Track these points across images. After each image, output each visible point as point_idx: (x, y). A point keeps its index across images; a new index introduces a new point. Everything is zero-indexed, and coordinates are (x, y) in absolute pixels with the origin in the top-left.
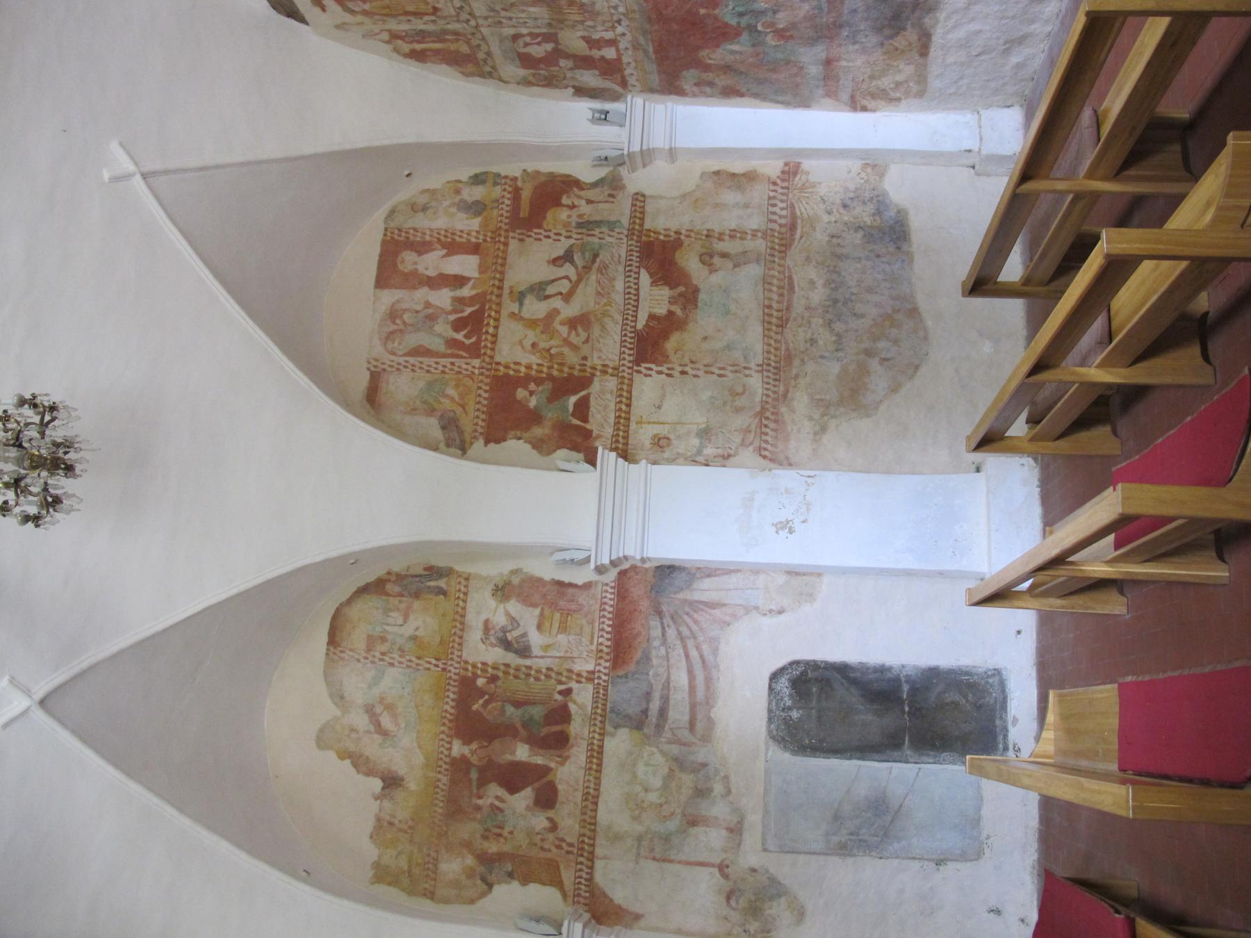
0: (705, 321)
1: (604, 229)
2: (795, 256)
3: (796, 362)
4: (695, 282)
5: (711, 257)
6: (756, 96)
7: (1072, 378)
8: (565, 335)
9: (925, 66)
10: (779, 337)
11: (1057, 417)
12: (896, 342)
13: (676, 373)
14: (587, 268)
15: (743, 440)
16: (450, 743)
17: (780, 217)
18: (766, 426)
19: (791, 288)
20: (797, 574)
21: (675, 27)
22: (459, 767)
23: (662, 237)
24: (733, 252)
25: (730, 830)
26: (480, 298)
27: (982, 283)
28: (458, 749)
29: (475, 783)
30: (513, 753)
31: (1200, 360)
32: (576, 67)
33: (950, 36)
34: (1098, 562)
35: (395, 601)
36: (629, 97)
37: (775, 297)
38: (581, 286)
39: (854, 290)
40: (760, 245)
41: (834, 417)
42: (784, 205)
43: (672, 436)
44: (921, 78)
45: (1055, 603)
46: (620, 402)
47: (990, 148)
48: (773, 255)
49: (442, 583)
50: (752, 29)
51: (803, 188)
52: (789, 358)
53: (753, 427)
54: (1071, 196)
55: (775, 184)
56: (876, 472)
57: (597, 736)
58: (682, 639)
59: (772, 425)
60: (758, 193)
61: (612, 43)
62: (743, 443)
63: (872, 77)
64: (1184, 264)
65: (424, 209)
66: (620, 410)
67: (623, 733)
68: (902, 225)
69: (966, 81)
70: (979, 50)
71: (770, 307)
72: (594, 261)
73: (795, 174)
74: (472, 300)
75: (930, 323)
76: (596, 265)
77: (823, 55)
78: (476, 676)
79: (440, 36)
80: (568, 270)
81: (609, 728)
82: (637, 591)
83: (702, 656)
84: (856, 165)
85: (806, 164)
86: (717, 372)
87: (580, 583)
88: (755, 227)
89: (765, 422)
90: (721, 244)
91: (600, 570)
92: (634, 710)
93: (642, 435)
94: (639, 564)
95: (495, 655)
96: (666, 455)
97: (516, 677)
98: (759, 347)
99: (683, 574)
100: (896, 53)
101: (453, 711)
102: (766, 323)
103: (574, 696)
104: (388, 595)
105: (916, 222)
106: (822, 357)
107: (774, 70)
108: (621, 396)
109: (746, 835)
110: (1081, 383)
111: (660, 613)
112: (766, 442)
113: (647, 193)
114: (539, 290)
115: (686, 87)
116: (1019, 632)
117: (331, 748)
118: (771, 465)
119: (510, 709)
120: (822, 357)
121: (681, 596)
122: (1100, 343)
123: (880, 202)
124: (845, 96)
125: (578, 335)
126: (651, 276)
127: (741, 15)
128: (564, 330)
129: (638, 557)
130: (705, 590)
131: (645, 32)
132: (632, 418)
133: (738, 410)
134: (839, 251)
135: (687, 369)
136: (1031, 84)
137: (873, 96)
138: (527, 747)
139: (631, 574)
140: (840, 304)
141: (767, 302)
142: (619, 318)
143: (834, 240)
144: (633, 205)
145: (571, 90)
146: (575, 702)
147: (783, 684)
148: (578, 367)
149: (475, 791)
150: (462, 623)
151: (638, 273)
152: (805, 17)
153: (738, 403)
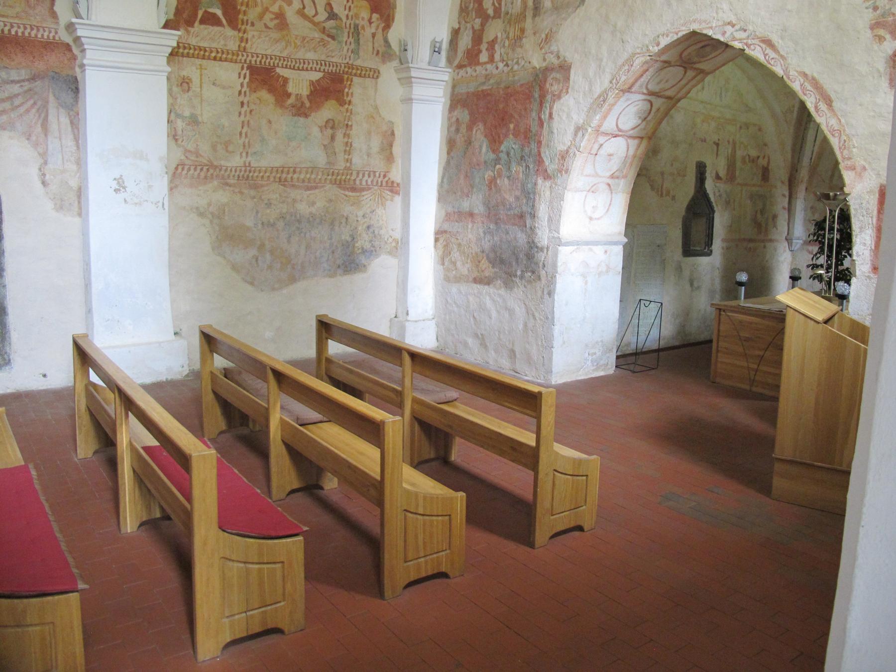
0: (284, 122)
1: (353, 46)
2: (333, 191)
3: (253, 193)
4: (313, 114)
5: (332, 128)
6: (448, 163)
7: (271, 400)
8: (271, 9)
9: (467, 282)
10: (272, 179)
11: (229, 389)
12: (270, 267)
13: (242, 98)
14: (323, 31)
15: (190, 151)
17: (361, 180)
18: (202, 169)
19: (308, 189)
20: (79, 197)
21: (501, 106)
23: (346, 90)
24: (335, 144)
27: (326, 328)
31: (289, 489)
32: (474, 31)
33: (488, 298)
34: (131, 435)
36: (450, 70)
37: (302, 176)
38: (310, 25)
39: (308, 235)
40: (341, 165)
41: (211, 222)
42: (369, 183)
43: (190, 93)
44: (458, 279)
45: (81, 403)
46: (218, 52)
47: (410, 327)
48: (333, 175)
50: (497, 161)
51: (381, 196)
52: (256, 187)
53: (200, 159)
54: (399, 389)
55: (385, 176)
56: (170, 258)
59: (203, 174)
60: (377, 164)
61: (491, 59)
62: (186, 151)
63: (459, 245)
64: (378, 478)
66: (211, 52)
68: (355, 269)
69: (456, 309)
70: (478, 317)
71: (294, 172)
72: (329, 36)
73: (392, 191)
75: (285, 291)
76: (326, 38)
77: (476, 211)
80: (322, 16)
82: (53, 60)
84: (397, 235)
85: (398, 199)
86: (244, 131)
87: (56, 8)
88: (354, 161)
89: (205, 168)
90: (342, 136)
91: (70, 27)
93: (190, 69)
94: (78, 62)
96: (175, 89)
98: (264, 163)
99: (72, 101)
100: (477, 262)
102: (282, 169)
105: (358, 277)
106: (257, 212)
107: (38, 110)
108: (223, 53)
110: (267, 409)
112: (189, 170)
113: (380, 80)
115: (456, 113)
116: (45, 376)
118: (171, 173)
120: (257, 212)
121: (51, 98)
122: (298, 419)
123: (371, 253)
124: (446, 226)
125: (272, 20)
126: (318, 81)
127: (508, 154)
128: (275, 8)
129: (85, 62)
130: (59, 119)
131: (498, 84)
132: (204, 61)
133: (214, 148)
134: (337, 223)
135: (245, 106)
136: (453, 353)
137: (446, 246)
139: (68, 55)
140: (297, 225)
141: (298, 170)
142: (285, 54)
143: (344, 221)
144: (371, 69)
145: (457, 26)
148: (245, 18)
151: (319, 71)
152: (505, 199)
153: (219, 147)
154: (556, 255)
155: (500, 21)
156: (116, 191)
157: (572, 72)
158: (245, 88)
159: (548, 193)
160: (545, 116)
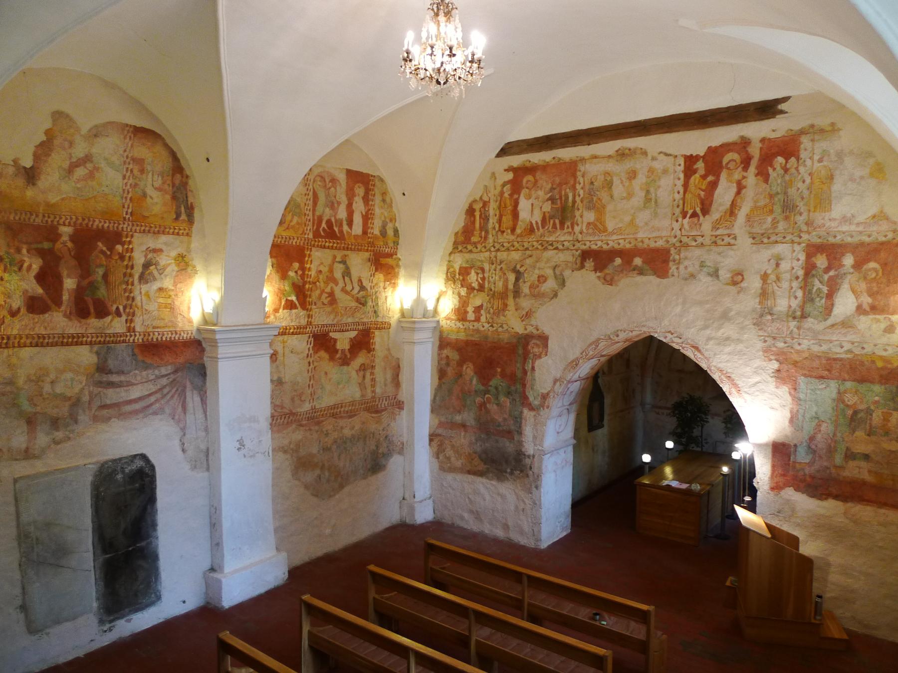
0: (334, 372)
3: (317, 428)
12: (328, 481)
13: (309, 359)
16: (69, 225)
19: (350, 417)
22: (52, 233)
25: (27, 450)
26: (342, 237)
28: (66, 231)
29: (39, 246)
30: (69, 276)
35: (169, 182)
44: (452, 470)
49: (183, 217)
50: (487, 392)
52: (318, 423)
57: (89, 339)
58: (161, 389)
61: (478, 319)
65: (384, 201)
67: (94, 359)
73: (399, 408)
74: (341, 231)
75: (337, 496)
77: (468, 424)
78: (123, 244)
79: (484, 228)
80: (357, 288)
81: (96, 348)
83: (152, 404)
85: (404, 413)
92: (111, 364)
95: (139, 259)
97: (125, 275)
98: (324, 405)
101: (95, 227)
102: (334, 407)
103: (117, 319)
104: (173, 175)
105: (380, 475)
109: (24, 463)
111: (176, 371)
114: (347, 273)
117: (54, 125)
119: (101, 271)
121: (188, 384)
123: (388, 455)
124: (440, 431)
128: (328, 290)
130: (192, 399)
138: (75, 287)
142: (335, 322)
146: (112, 321)
147: (139, 463)
149: (34, 246)
150: (159, 232)
153: (296, 399)
154: (541, 461)
155: (482, 294)
156: (239, 449)
157: (550, 342)
158: (311, 351)
159: (532, 420)
160: (528, 367)
